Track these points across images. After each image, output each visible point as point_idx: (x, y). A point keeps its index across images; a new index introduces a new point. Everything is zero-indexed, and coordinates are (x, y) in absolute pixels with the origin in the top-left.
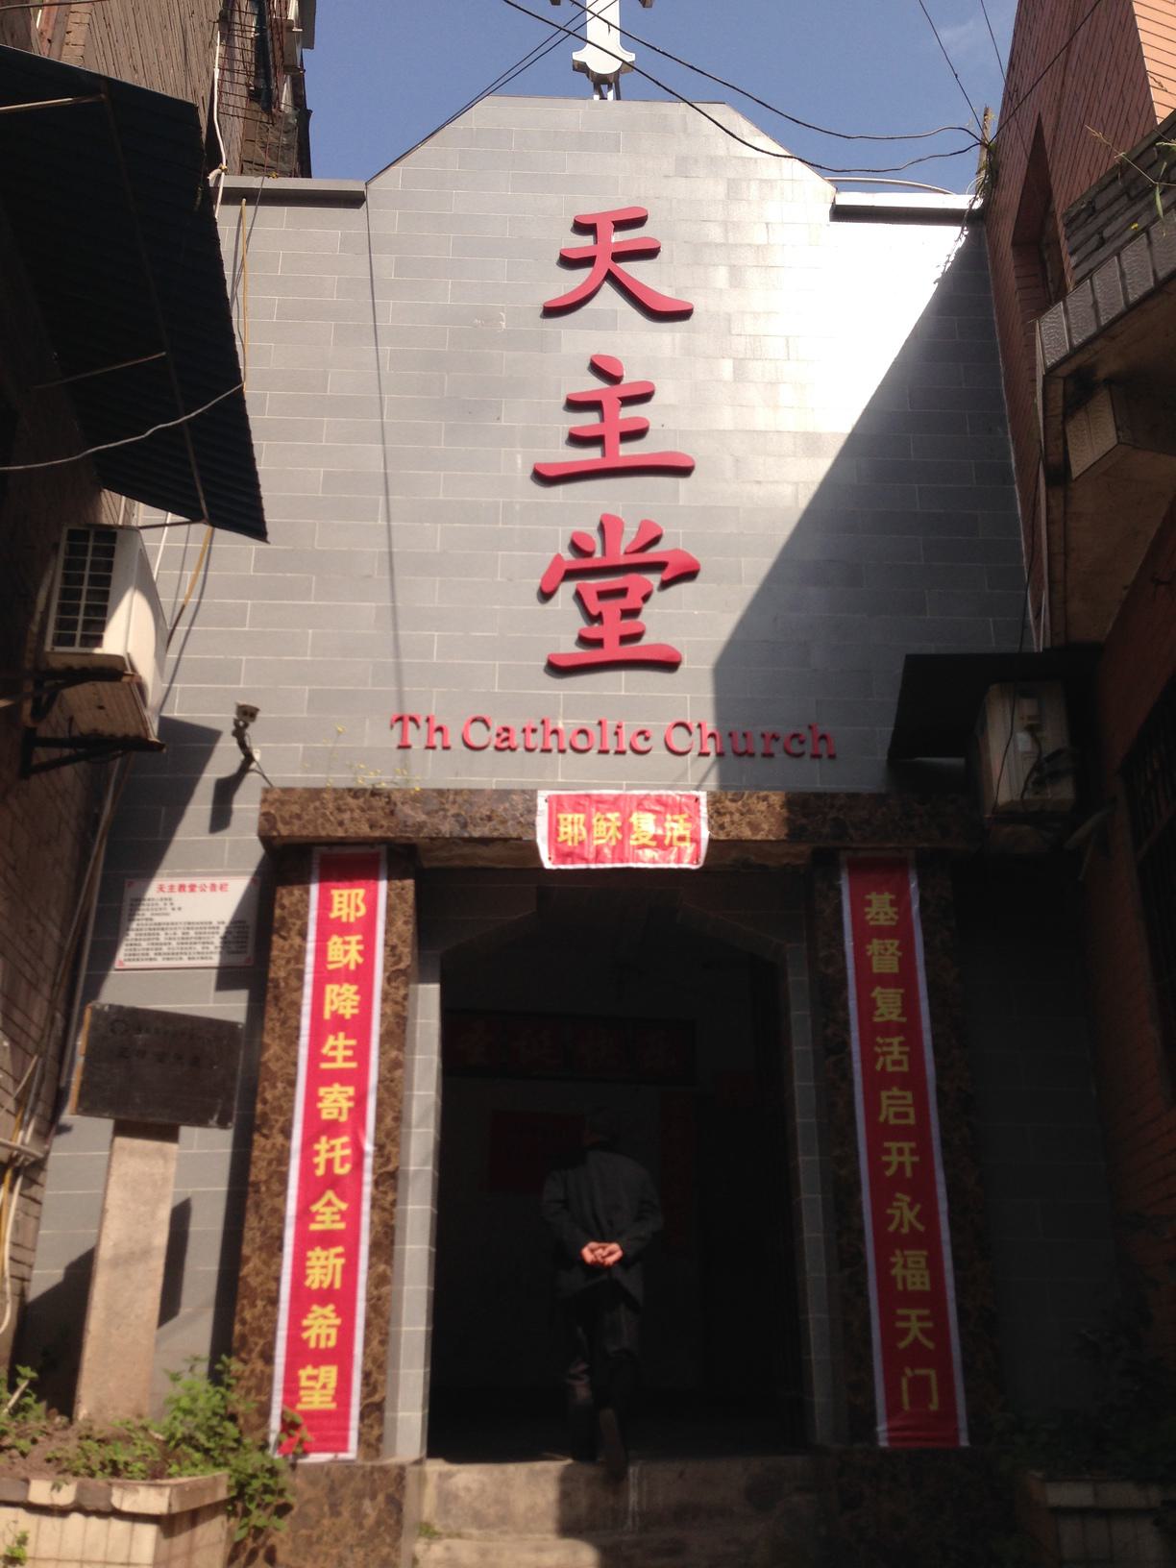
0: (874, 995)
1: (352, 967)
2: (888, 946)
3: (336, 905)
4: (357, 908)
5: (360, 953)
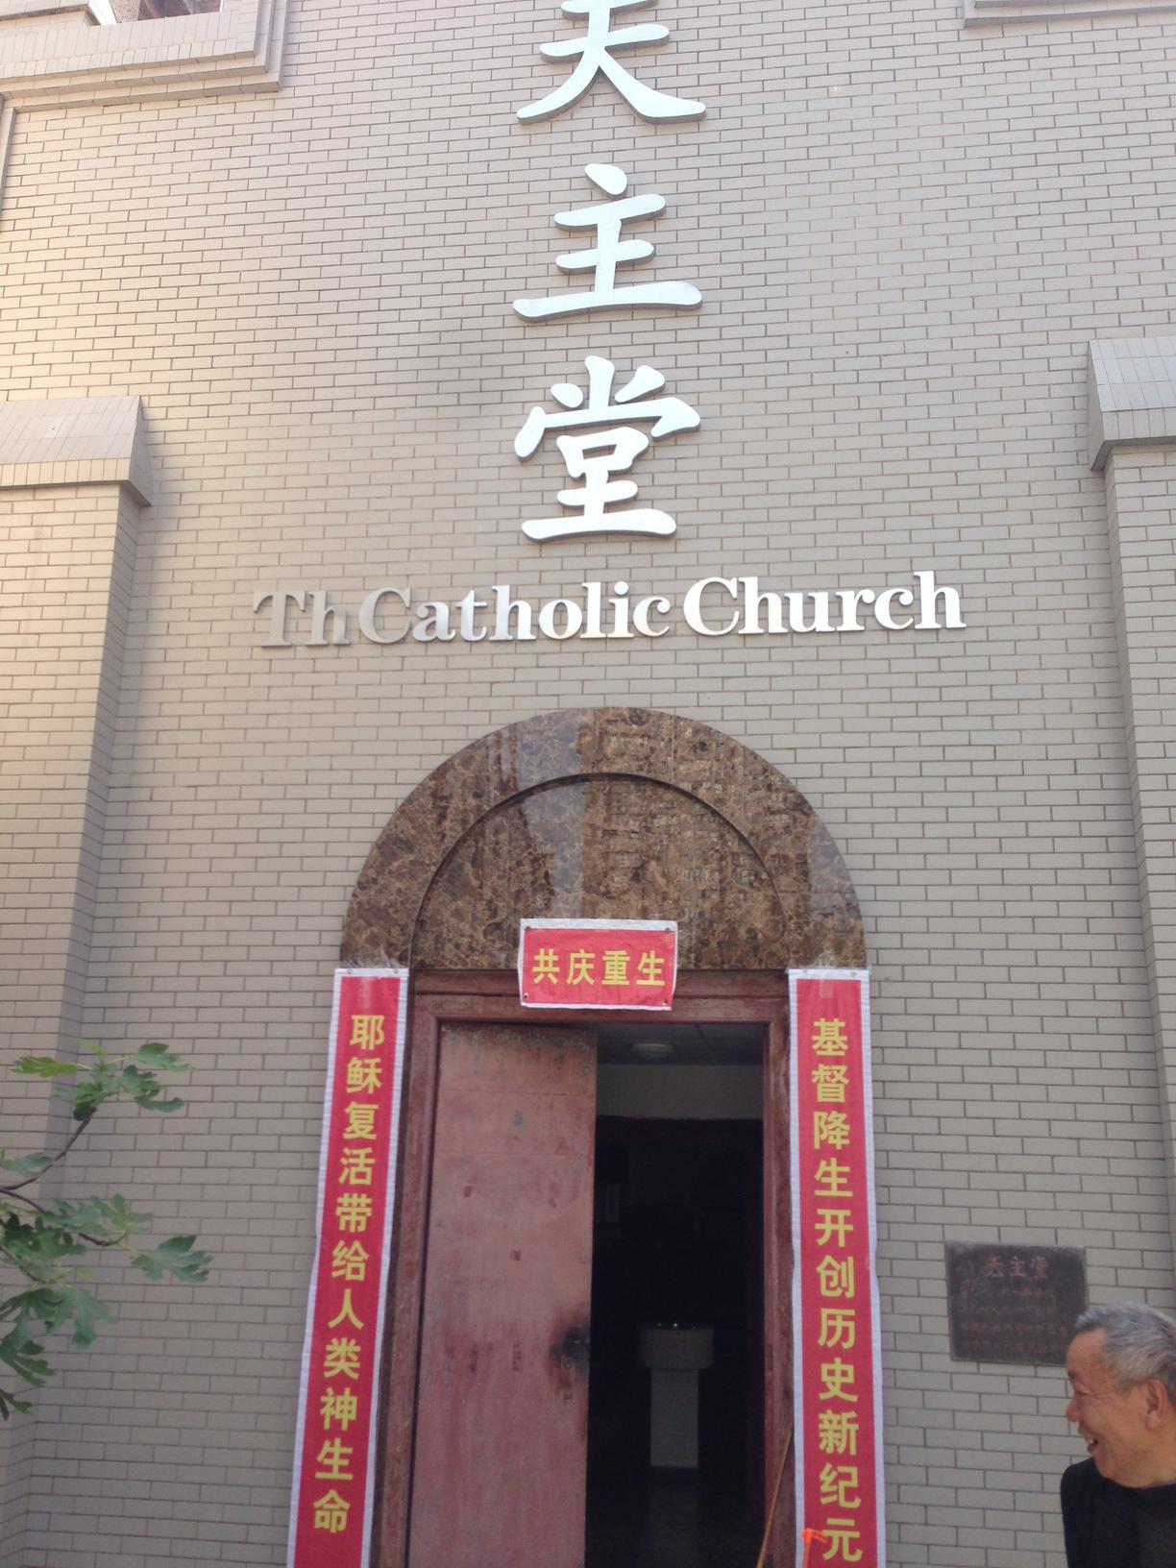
0: (347, 1110)
1: (371, 1091)
2: (835, 1073)
3: (356, 1032)
4: (377, 1036)
5: (378, 1076)
